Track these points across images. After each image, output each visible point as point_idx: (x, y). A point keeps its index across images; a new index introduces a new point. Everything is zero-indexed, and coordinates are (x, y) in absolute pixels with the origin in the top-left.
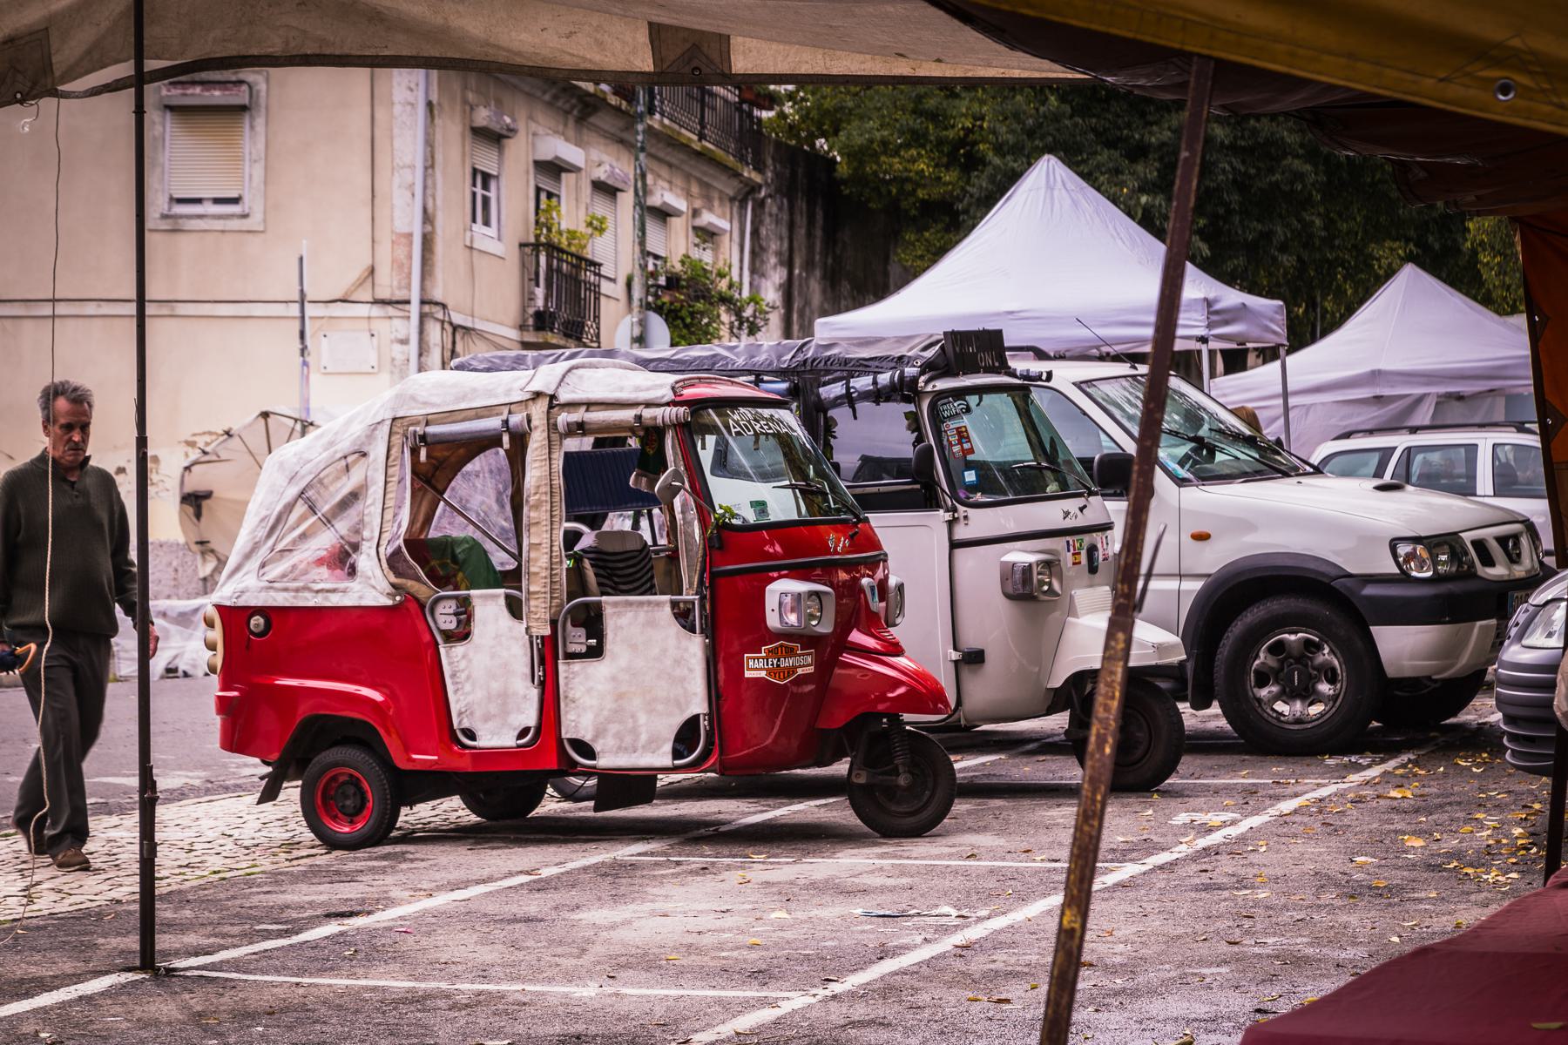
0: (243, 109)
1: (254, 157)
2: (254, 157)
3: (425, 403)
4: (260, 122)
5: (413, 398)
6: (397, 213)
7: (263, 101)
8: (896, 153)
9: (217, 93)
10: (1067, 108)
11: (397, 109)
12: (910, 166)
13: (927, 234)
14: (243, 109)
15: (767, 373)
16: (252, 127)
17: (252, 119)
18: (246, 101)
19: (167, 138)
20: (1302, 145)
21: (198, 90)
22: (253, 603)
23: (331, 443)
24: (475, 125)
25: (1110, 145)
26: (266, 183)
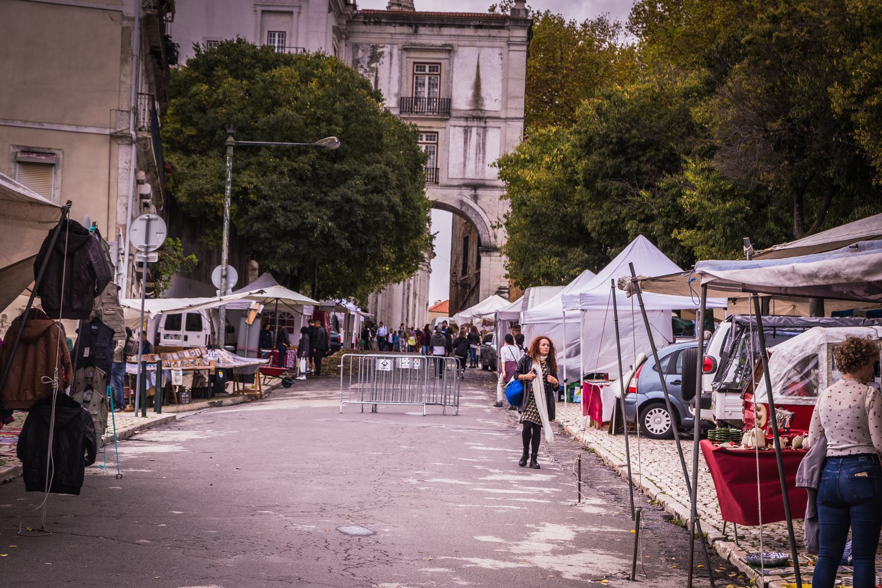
0: (53, 165)
1: (56, 186)
2: (56, 186)
3: (837, 339)
4: (59, 172)
5: (832, 337)
6: (119, 216)
7: (61, 163)
8: (211, 195)
9: (43, 158)
10: (294, 182)
11: (120, 171)
12: (216, 201)
13: (216, 231)
14: (53, 165)
15: (778, 327)
16: (55, 173)
17: (56, 170)
18: (54, 162)
19: (17, 175)
20: (388, 207)
21: (35, 156)
22: (780, 403)
23: (802, 351)
24: (139, 179)
25: (306, 199)
26: (61, 198)
